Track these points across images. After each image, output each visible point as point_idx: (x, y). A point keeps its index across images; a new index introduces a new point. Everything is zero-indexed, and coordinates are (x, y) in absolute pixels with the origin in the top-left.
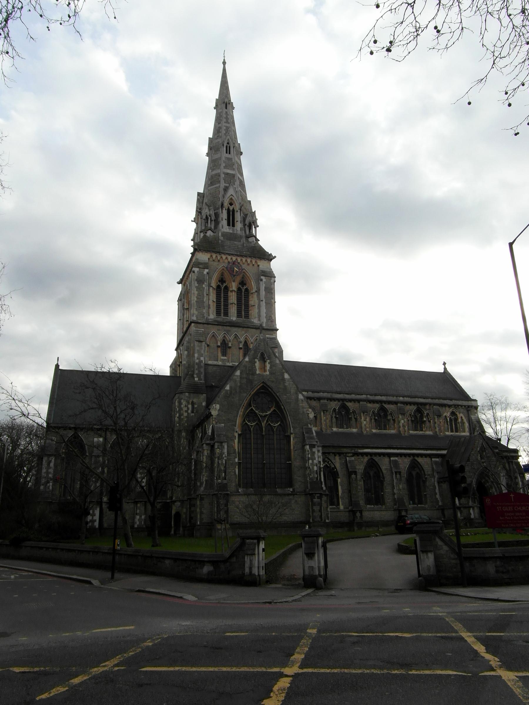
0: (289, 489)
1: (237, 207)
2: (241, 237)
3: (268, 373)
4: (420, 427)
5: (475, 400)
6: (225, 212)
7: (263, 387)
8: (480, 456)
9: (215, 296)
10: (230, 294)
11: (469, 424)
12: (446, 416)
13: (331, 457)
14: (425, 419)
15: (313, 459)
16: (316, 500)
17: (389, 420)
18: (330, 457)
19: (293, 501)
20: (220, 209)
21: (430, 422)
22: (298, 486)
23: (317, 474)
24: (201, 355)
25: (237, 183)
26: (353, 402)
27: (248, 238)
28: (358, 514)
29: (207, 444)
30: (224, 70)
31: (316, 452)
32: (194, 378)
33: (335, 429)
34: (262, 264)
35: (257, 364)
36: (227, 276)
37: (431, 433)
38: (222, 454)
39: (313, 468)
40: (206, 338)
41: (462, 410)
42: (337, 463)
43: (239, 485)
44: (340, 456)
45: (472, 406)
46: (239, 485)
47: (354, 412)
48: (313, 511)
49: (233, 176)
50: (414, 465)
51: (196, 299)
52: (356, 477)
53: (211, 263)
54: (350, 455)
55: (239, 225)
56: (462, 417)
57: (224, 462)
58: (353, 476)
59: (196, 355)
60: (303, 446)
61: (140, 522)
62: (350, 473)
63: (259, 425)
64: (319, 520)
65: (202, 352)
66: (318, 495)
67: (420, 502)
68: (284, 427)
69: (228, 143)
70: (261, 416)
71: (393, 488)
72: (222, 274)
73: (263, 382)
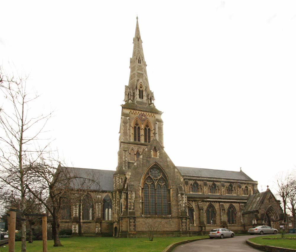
0: (169, 215)
1: (144, 89)
2: (146, 104)
3: (158, 157)
4: (231, 193)
5: (257, 182)
6: (138, 91)
7: (155, 165)
8: (269, 201)
9: (133, 131)
10: (141, 131)
11: (253, 191)
12: (243, 188)
13: (191, 202)
14: (233, 189)
15: (183, 201)
16: (184, 220)
17: (217, 189)
18: (190, 202)
19: (171, 221)
20: (136, 90)
21: (235, 190)
22: (174, 214)
23: (184, 208)
24: (126, 157)
25: (144, 78)
26: (200, 181)
27: (150, 104)
28: (204, 228)
29: (124, 193)
30: (137, 22)
31: (184, 197)
32: (123, 168)
33: (191, 193)
34: (157, 116)
35: (152, 153)
36: (139, 122)
37: (236, 195)
38: (132, 197)
39: (182, 205)
40: (129, 150)
41: (250, 186)
42: (194, 205)
43: (142, 213)
44: (195, 202)
45: (255, 184)
46: (142, 213)
47: (200, 185)
48: (182, 226)
49: (142, 74)
50: (231, 207)
51: (123, 131)
52: (203, 211)
53: (131, 115)
54: (200, 201)
55: (145, 98)
56: (250, 189)
57: (133, 201)
58: (202, 211)
59: (123, 157)
60: (177, 195)
61: (98, 231)
62: (200, 209)
63: (153, 184)
64: (185, 230)
65: (127, 156)
66: (185, 218)
67: (233, 223)
68: (167, 185)
69: (139, 58)
70: (154, 180)
71: (221, 216)
72: (137, 121)
73: (155, 162)
